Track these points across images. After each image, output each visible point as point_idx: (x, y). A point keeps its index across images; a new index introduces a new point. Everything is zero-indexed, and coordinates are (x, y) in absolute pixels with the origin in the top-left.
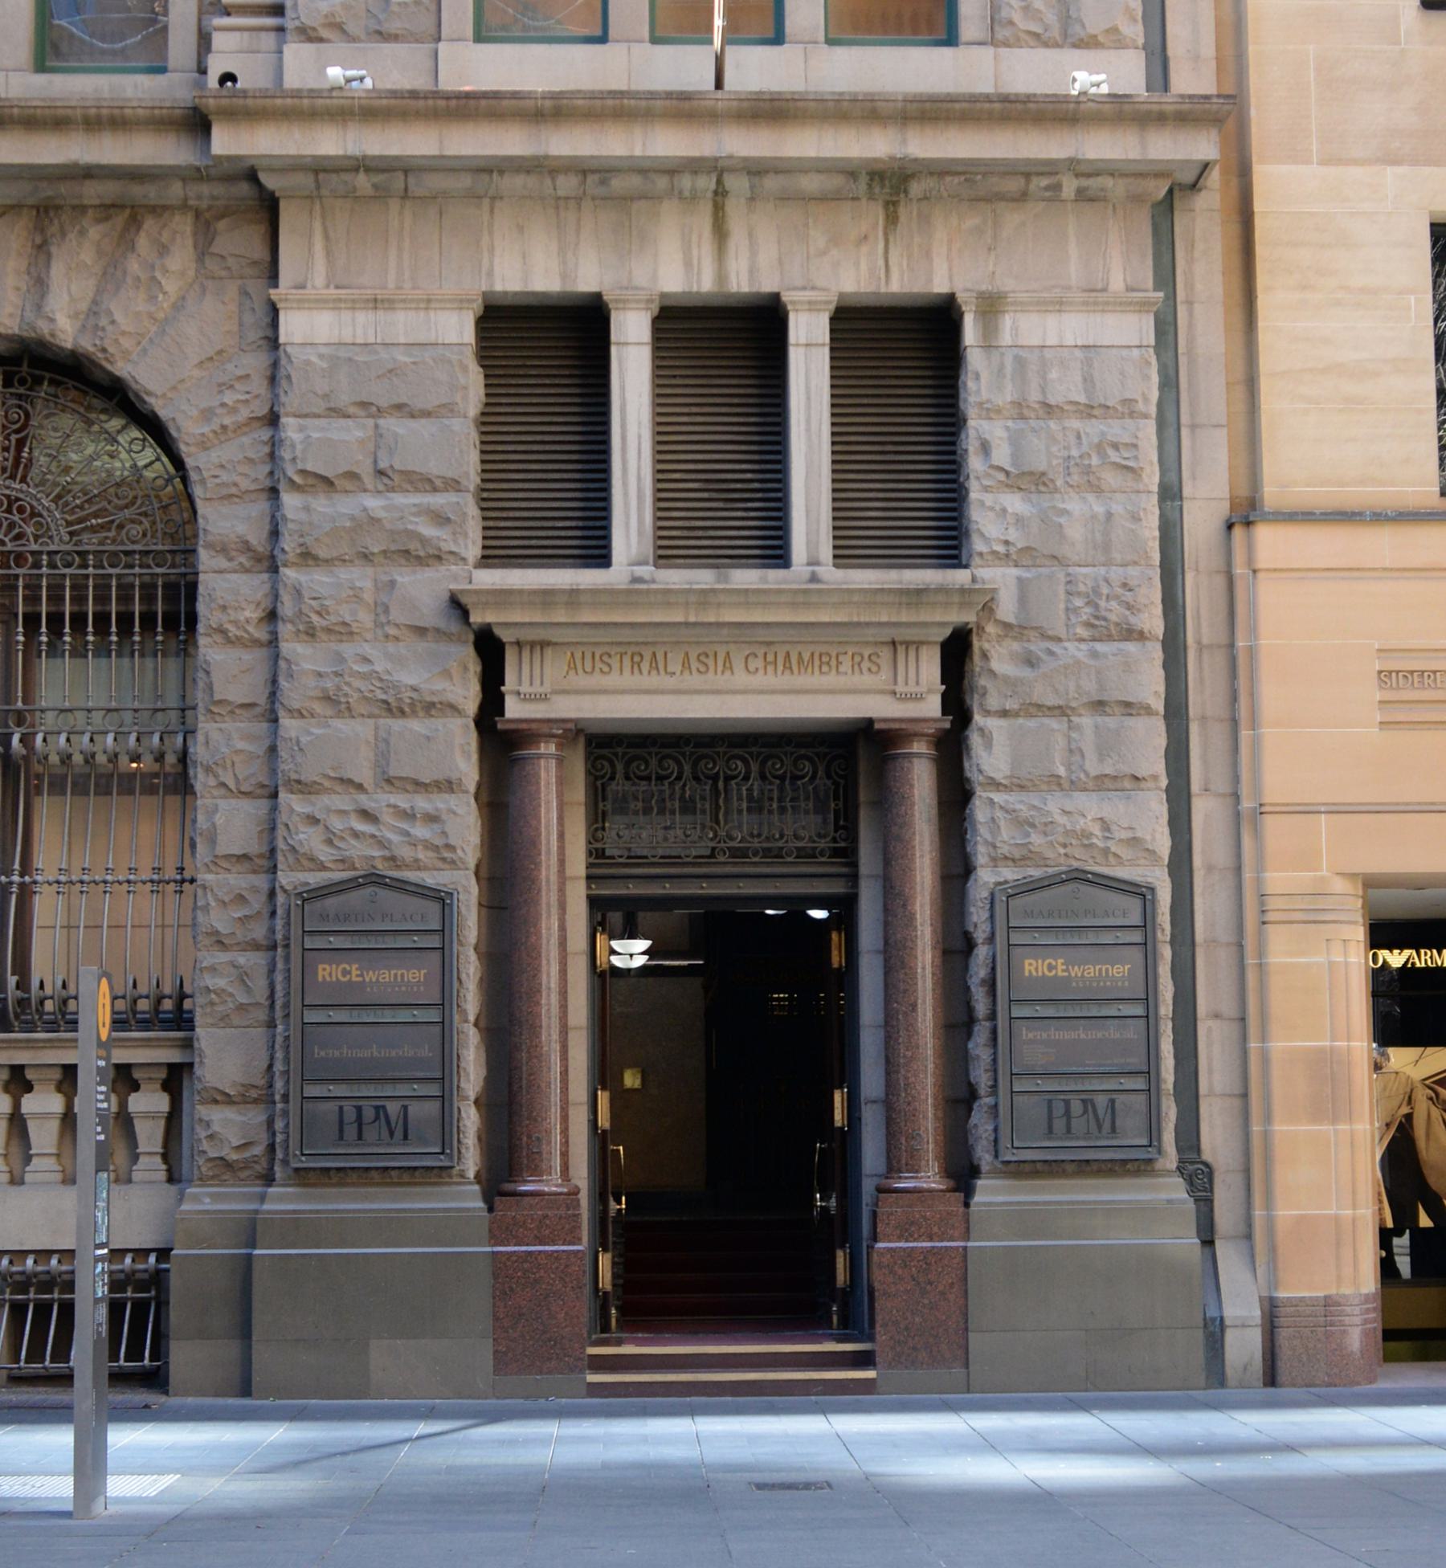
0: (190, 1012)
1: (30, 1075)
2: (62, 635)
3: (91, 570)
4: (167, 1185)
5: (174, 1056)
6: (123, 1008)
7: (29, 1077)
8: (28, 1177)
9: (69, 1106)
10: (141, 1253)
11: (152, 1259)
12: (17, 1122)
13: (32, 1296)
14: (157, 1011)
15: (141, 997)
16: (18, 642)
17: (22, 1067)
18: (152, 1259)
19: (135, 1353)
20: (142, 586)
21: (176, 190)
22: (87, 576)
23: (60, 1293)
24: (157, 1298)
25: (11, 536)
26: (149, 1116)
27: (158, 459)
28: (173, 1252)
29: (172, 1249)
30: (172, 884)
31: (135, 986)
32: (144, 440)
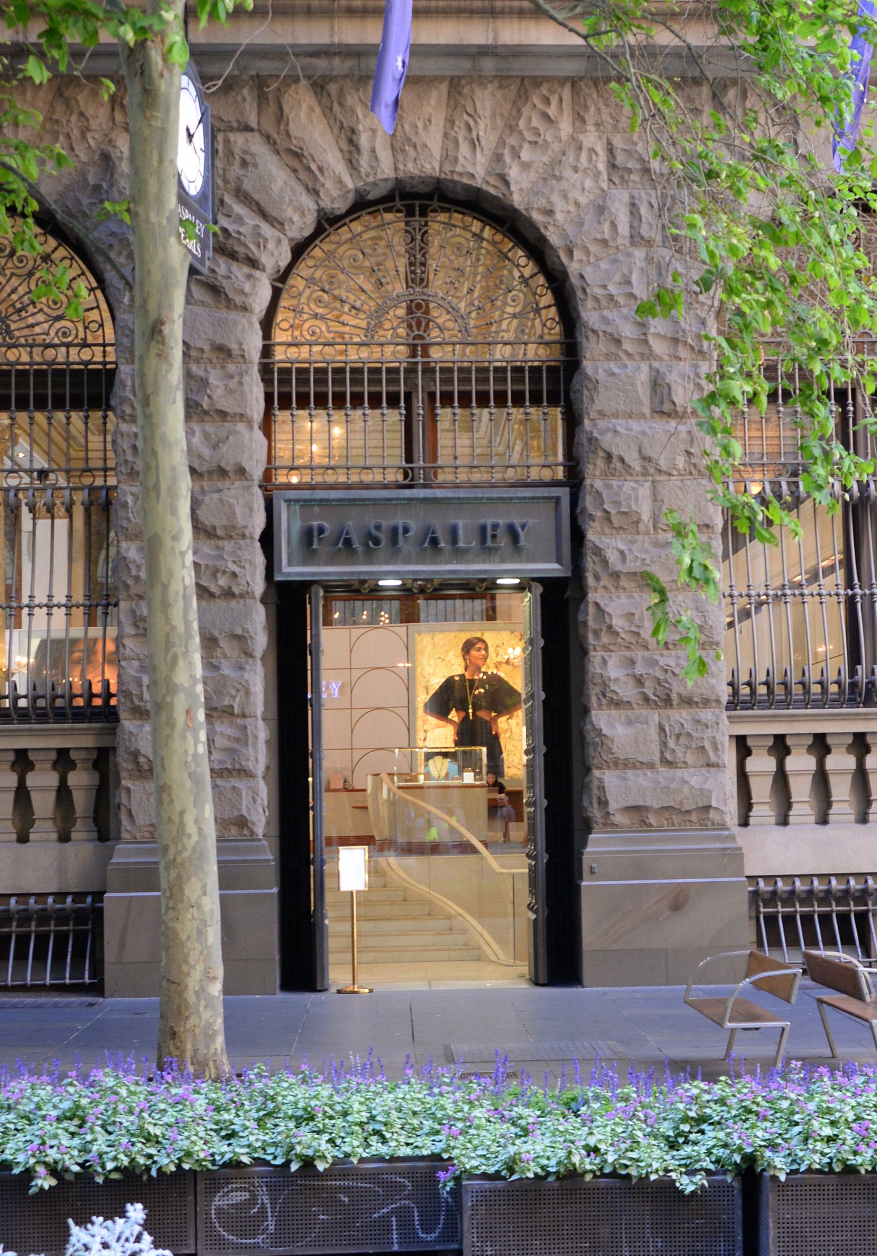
0: (114, 707)
1: (32, 757)
2: (847, 405)
3: (419, 359)
4: (99, 843)
5: (104, 742)
6: (44, 705)
7: (31, 758)
8: (32, 837)
9: (861, 764)
10: (79, 896)
11: (89, 899)
12: (22, 795)
13: (52, 928)
14: (35, 708)
15: (58, 697)
16: (419, 414)
17: (25, 751)
18: (89, 899)
19: (77, 970)
20: (478, 370)
21: (298, 64)
22: (417, 363)
23: (74, 925)
24: (93, 929)
25: (415, 328)
26: (842, 773)
27: (83, 273)
28: (106, 895)
29: (105, 892)
30: (81, 608)
31: (53, 689)
32: (72, 259)
